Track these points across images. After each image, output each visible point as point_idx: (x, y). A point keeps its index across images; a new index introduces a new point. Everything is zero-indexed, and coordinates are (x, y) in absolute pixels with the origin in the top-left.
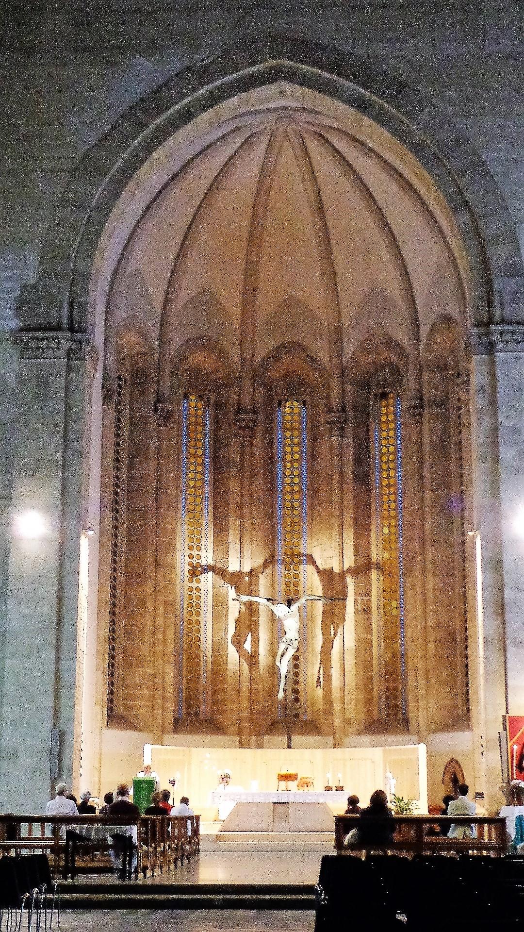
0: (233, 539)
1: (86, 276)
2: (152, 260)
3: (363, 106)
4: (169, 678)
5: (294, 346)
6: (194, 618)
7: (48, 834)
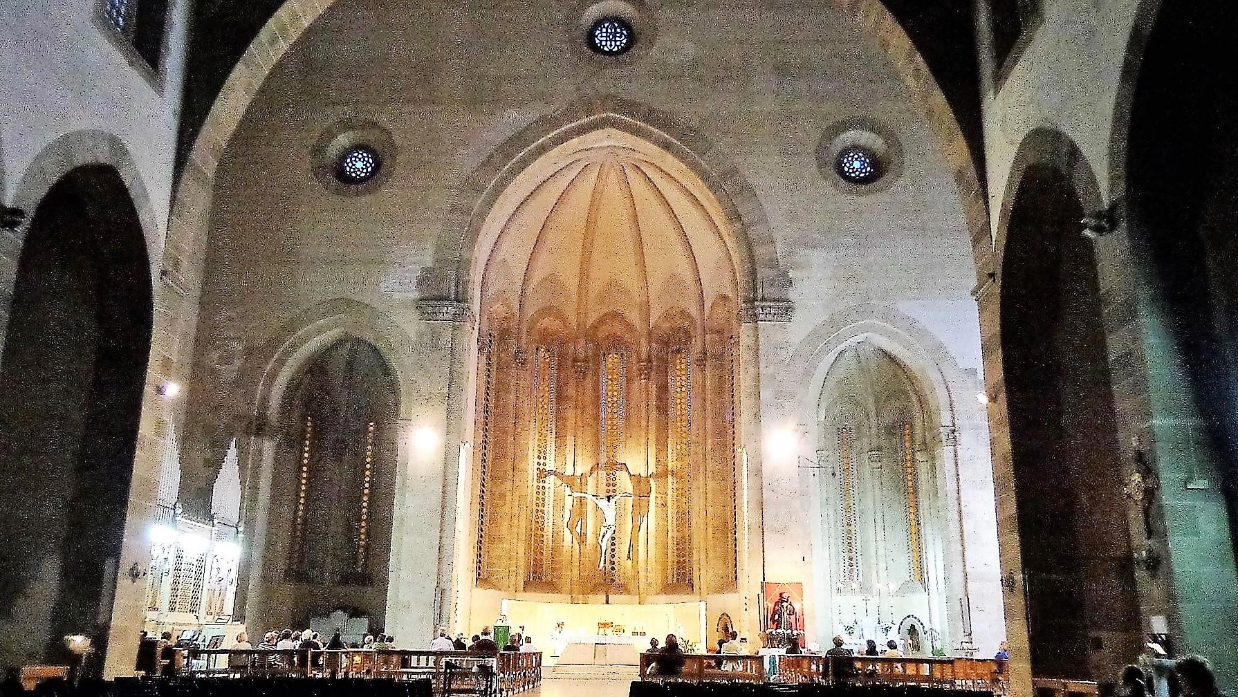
0: (570, 441)
1: (469, 262)
2: (515, 253)
3: (667, 146)
4: (522, 551)
5: (615, 315)
6: (539, 532)
7: (431, 664)
